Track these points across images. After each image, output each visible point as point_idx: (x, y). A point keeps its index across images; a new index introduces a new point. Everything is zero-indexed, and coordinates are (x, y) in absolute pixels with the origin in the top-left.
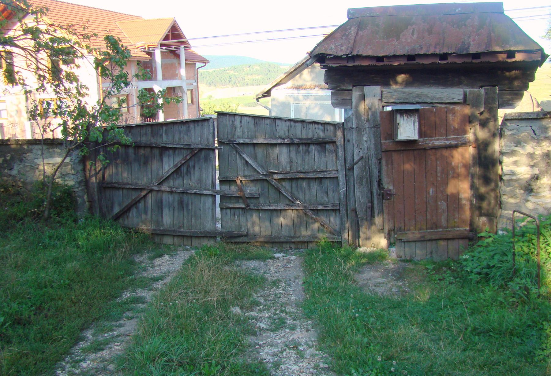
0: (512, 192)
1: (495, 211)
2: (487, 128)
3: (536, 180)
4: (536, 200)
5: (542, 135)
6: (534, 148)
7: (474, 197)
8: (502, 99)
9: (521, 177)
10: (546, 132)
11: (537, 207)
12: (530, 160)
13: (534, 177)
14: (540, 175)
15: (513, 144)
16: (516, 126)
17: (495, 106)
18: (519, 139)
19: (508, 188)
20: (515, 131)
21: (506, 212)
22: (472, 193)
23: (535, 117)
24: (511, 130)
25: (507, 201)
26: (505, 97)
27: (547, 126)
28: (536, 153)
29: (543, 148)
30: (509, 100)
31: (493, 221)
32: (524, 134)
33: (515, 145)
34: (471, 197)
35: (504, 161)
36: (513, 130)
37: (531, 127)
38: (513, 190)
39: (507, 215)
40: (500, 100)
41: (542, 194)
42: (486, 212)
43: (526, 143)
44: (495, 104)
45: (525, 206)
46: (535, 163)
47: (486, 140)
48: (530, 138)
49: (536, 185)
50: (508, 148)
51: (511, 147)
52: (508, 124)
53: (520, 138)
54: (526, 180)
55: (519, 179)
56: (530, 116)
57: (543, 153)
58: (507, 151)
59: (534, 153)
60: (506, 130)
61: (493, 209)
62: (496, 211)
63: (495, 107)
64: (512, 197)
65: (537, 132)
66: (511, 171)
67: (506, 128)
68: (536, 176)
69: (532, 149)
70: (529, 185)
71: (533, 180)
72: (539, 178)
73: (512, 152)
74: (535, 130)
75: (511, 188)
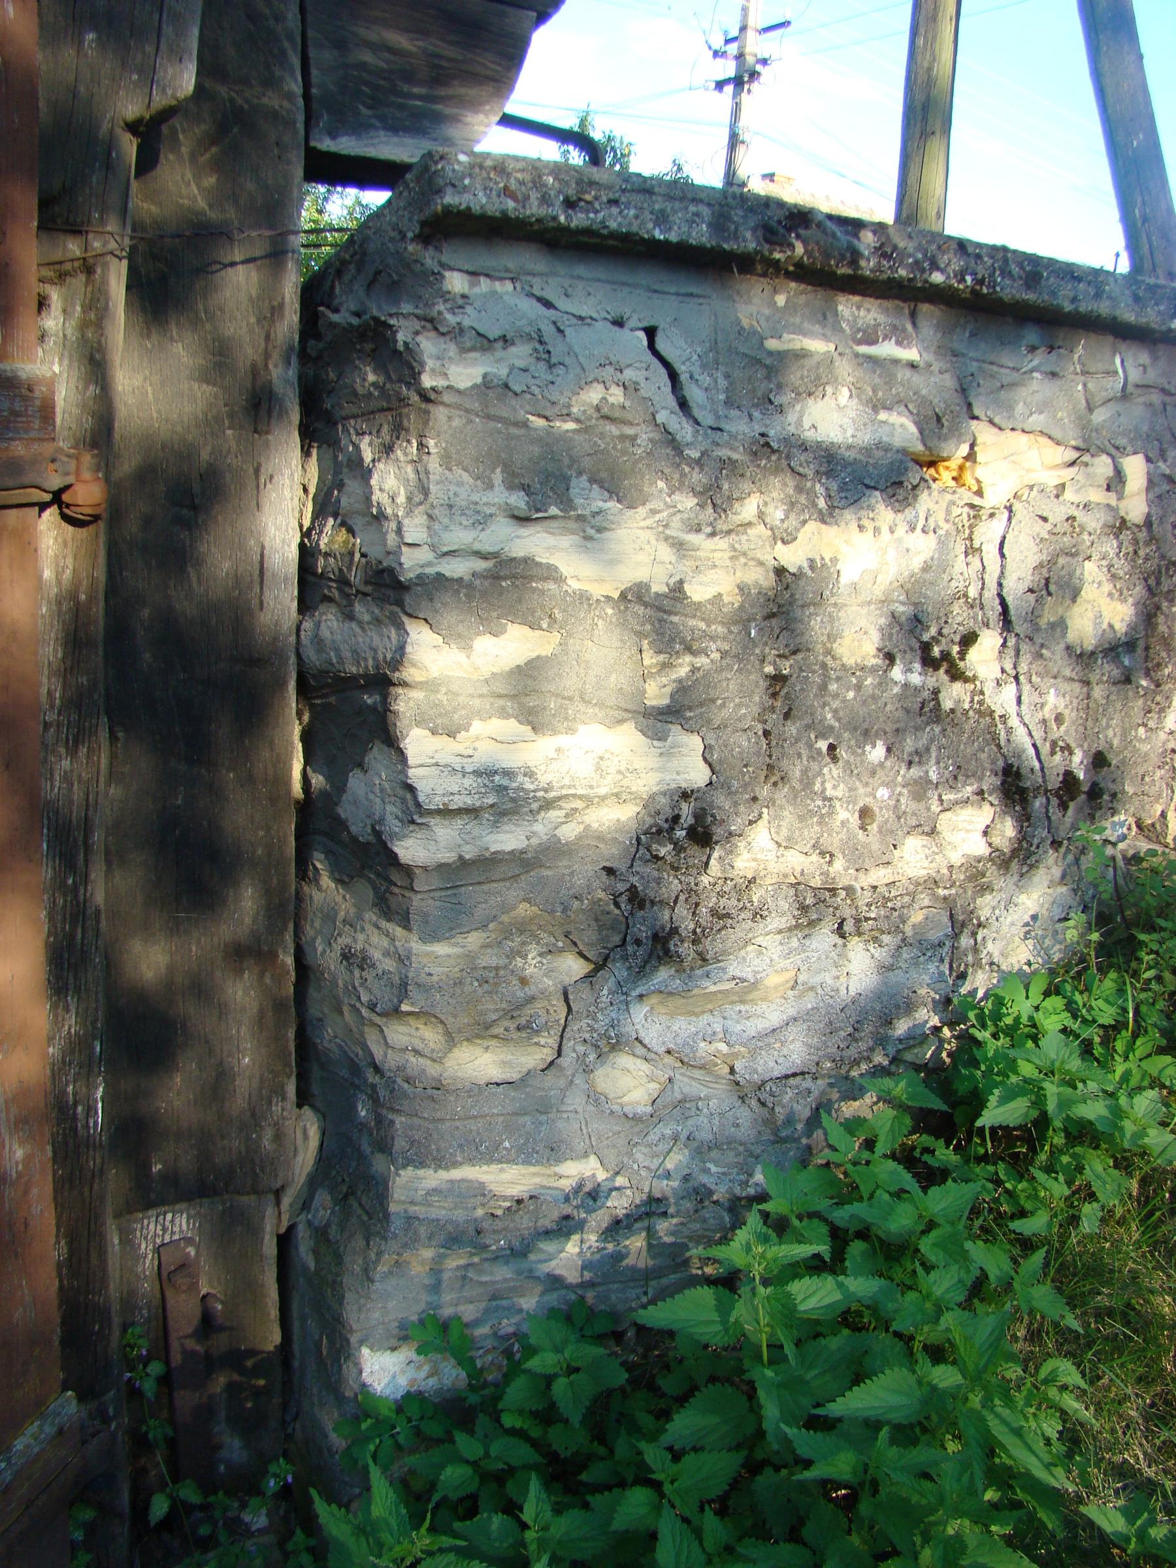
0: (490, 979)
1: (267, 1143)
2: (196, 323)
3: (695, 853)
4: (684, 1027)
5: (741, 426)
6: (679, 546)
7: (87, 1069)
8: (341, 45)
9: (569, 832)
10: (768, 404)
11: (688, 1084)
12: (650, 659)
13: (676, 819)
14: (721, 800)
15: (500, 496)
16: (529, 307)
17: (272, 101)
18: (551, 444)
19: (441, 949)
20: (520, 354)
21: (432, 1178)
22: (71, 1024)
23: (701, 235)
24: (485, 343)
25: (433, 1070)
26: (375, 34)
27: (772, 344)
28: (698, 592)
29: (743, 541)
30: (409, 76)
31: (254, 1232)
32: (594, 395)
33: (518, 500)
34: (58, 1070)
35: (409, 673)
36: (505, 340)
37: (651, 332)
38: (490, 959)
39: (440, 1211)
40: (322, 56)
41: (734, 969)
42: (186, 1161)
43: (613, 491)
44: (271, 82)
45: (595, 1098)
46: (682, 689)
47: (185, 453)
48: (645, 435)
49: (692, 894)
50: (460, 536)
51: (482, 521)
52: (456, 282)
53: (564, 437)
54: (612, 854)
55: (553, 850)
56: (662, 219)
57: (741, 588)
58: (456, 568)
59: (677, 590)
60: (428, 345)
61: (255, 1117)
62: (278, 1137)
63: (275, 116)
64: (481, 1031)
65: (695, 394)
66: (486, 773)
67: (432, 323)
68: (686, 811)
69: (666, 553)
70: (637, 899)
71: (664, 850)
72: (718, 832)
73: (494, 577)
74: (682, 369)
75: (474, 940)
